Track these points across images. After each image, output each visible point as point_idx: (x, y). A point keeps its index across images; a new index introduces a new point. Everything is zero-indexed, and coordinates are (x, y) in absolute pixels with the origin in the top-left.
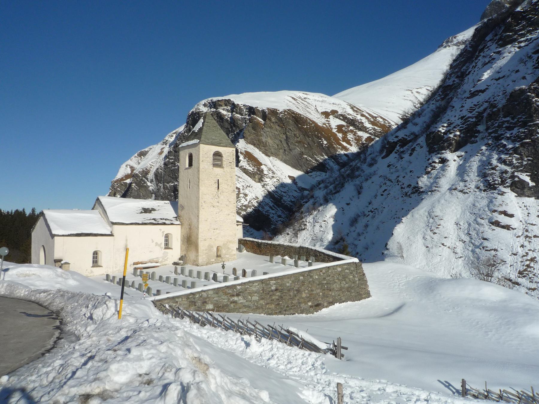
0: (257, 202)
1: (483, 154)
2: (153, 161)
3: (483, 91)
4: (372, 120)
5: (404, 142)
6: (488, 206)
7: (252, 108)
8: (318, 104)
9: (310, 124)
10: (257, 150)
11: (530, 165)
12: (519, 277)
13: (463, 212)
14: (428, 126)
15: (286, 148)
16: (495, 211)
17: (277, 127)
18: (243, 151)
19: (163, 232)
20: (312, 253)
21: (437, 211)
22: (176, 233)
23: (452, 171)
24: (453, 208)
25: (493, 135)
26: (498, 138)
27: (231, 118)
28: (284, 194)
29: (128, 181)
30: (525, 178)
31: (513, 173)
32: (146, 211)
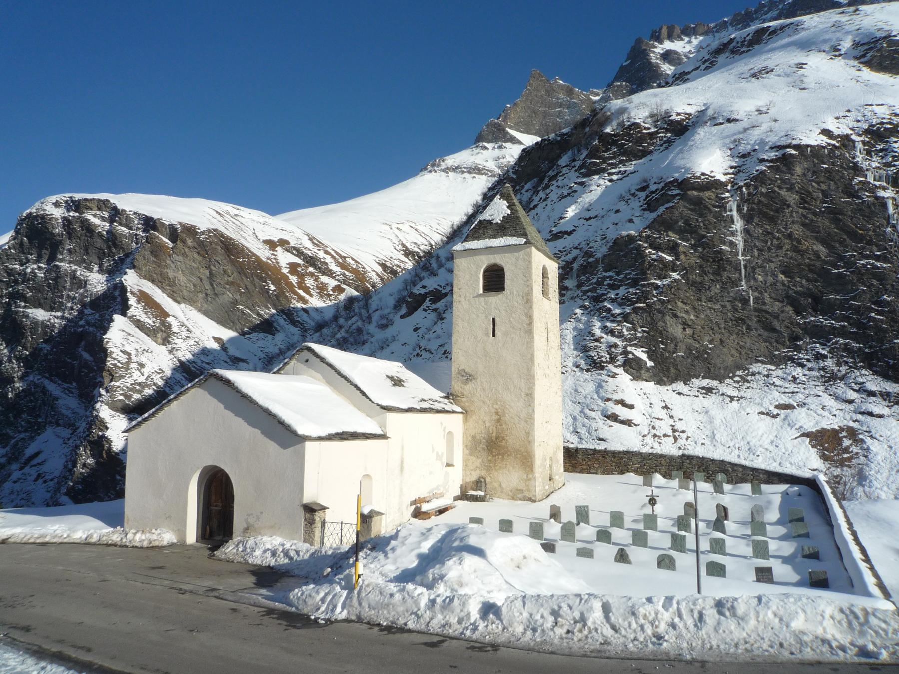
0: (161, 378)
3: (569, 233)
4: (340, 260)
6: (597, 393)
7: (152, 219)
8: (259, 228)
9: (249, 257)
15: (209, 292)
16: (609, 400)
17: (196, 256)
18: (135, 290)
25: (589, 294)
26: (597, 299)
28: (207, 366)
30: (641, 354)
31: (625, 347)
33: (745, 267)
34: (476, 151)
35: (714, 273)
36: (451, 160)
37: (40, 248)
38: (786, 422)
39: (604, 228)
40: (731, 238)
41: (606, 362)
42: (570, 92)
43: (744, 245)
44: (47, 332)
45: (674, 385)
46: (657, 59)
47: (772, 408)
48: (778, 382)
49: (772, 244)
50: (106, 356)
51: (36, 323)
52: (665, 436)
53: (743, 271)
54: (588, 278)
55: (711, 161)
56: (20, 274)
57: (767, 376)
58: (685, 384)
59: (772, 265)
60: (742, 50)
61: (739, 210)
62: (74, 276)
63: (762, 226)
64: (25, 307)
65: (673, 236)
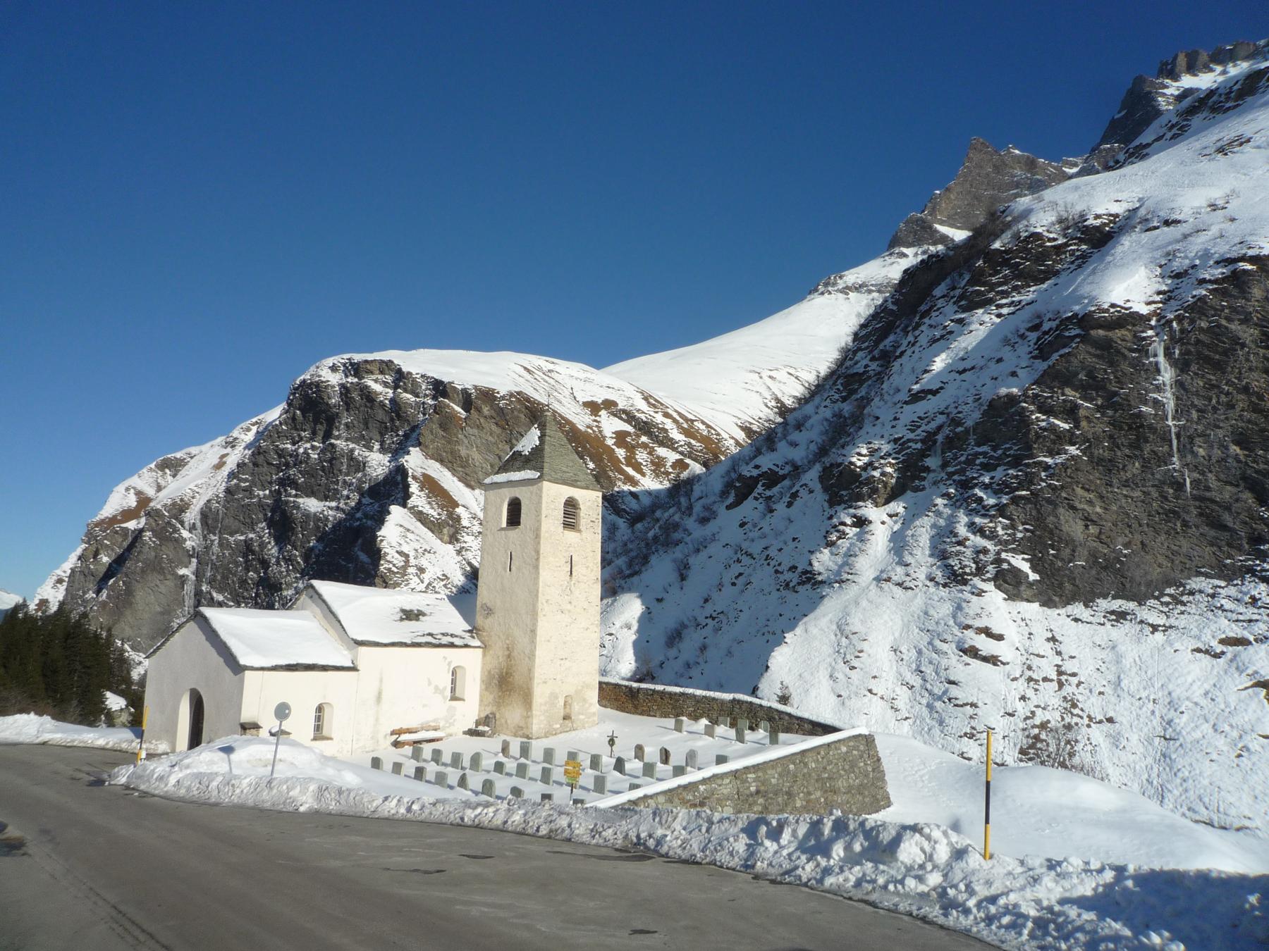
1: (939, 514)
2: (199, 482)
3: (934, 393)
4: (685, 426)
5: (772, 479)
6: (954, 617)
7: (442, 382)
8: (578, 386)
10: (448, 474)
11: (1029, 539)
12: (1021, 760)
13: (906, 626)
14: (823, 451)
16: (968, 627)
17: (494, 427)
18: (418, 475)
19: (449, 663)
20: (761, 714)
21: (855, 624)
22: (472, 662)
23: (880, 544)
24: (886, 617)
25: (956, 477)
26: (965, 485)
27: (392, 401)
29: (132, 525)
30: (1021, 563)
31: (998, 553)
32: (410, 615)
33: (1178, 436)
34: (889, 260)
35: (1130, 446)
36: (852, 276)
37: (316, 421)
38: (1234, 665)
39: (979, 385)
40: (1155, 396)
41: (971, 574)
42: (1031, 165)
43: (1177, 405)
44: (318, 527)
45: (1069, 607)
46: (1169, 104)
47: (1214, 643)
48: (1228, 605)
49: (1218, 402)
50: (379, 558)
51: (307, 515)
52: (1045, 679)
53: (1175, 442)
54: (955, 455)
55: (1129, 286)
56: (291, 456)
57: (1213, 596)
58: (1086, 606)
59: (1220, 433)
60: (1227, 105)
61: (1168, 354)
62: (351, 458)
63: (1203, 376)
64: (296, 496)
65: (1071, 395)
